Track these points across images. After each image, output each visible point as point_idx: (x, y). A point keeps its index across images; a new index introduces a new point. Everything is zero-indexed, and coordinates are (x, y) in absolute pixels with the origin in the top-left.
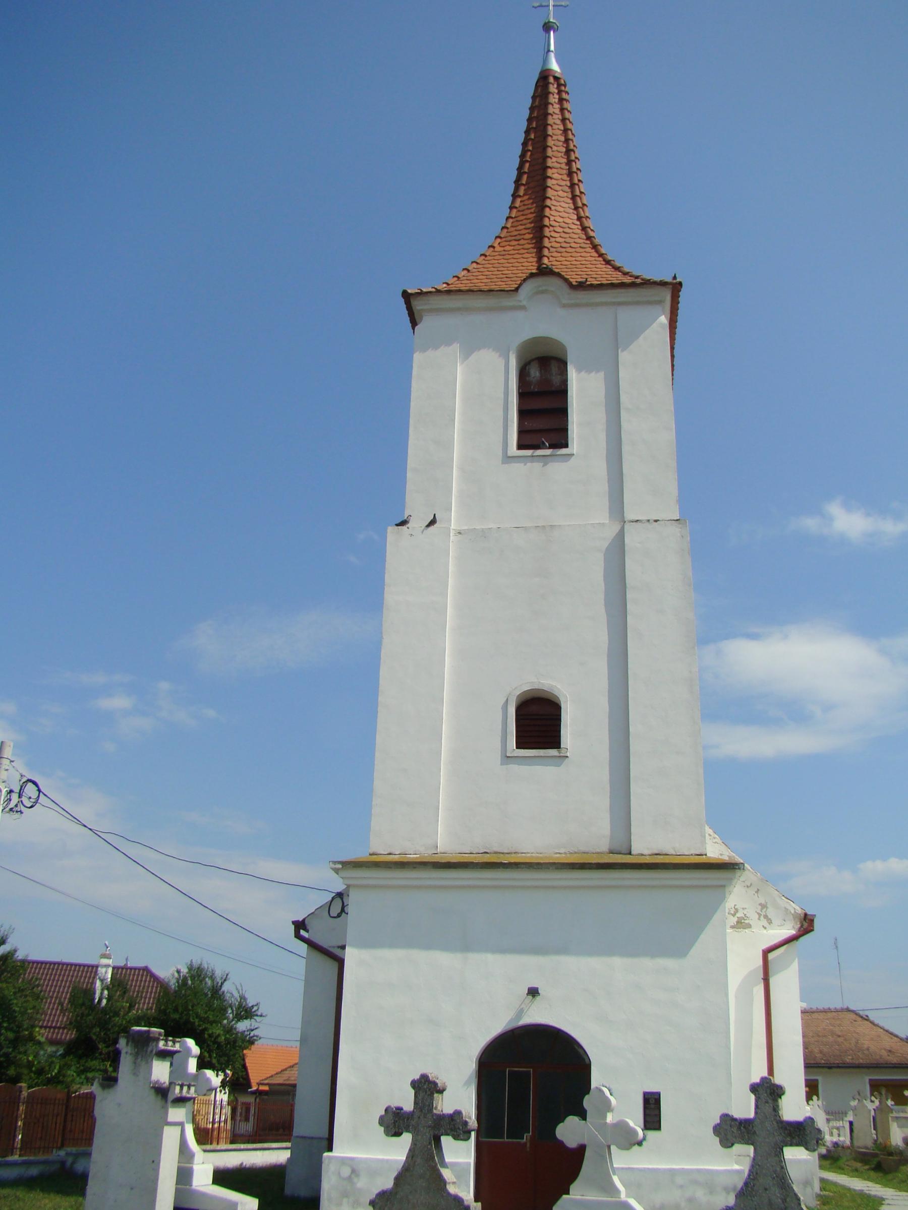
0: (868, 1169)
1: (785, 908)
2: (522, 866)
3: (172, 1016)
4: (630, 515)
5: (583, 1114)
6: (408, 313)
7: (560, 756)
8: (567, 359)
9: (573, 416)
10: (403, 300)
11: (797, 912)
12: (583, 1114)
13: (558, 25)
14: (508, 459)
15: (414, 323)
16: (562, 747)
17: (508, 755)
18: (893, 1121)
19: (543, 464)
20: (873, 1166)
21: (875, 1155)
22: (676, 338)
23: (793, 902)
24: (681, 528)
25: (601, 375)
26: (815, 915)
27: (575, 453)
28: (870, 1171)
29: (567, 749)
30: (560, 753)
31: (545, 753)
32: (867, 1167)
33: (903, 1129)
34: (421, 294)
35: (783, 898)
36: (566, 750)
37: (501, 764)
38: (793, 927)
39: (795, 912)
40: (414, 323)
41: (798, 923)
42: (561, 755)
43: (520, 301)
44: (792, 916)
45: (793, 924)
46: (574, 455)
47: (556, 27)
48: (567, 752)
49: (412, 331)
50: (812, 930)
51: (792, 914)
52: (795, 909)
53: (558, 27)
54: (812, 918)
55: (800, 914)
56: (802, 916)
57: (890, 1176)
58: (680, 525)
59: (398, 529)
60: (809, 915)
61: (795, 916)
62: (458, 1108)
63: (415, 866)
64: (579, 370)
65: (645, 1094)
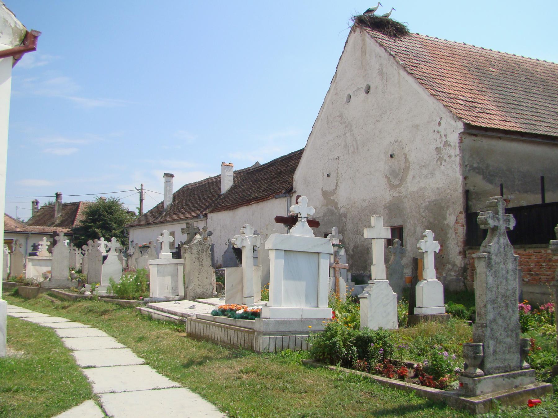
0: (9, 295)
1: (4, 19)
3: (444, 273)
5: (104, 240)
11: (18, 27)
12: (104, 240)
18: (29, 262)
20: (12, 293)
21: (14, 285)
23: (15, 16)
25: (304, 283)
26: (40, 32)
28: (10, 297)
32: (8, 293)
33: (37, 267)
35: (4, 8)
38: (11, 43)
39: (16, 26)
41: (18, 40)
44: (11, 31)
45: (11, 40)
50: (34, 49)
51: (12, 28)
52: (16, 23)
54: (36, 35)
55: (21, 30)
56: (24, 33)
57: (32, 301)
61: (15, 30)
65: (173, 258)
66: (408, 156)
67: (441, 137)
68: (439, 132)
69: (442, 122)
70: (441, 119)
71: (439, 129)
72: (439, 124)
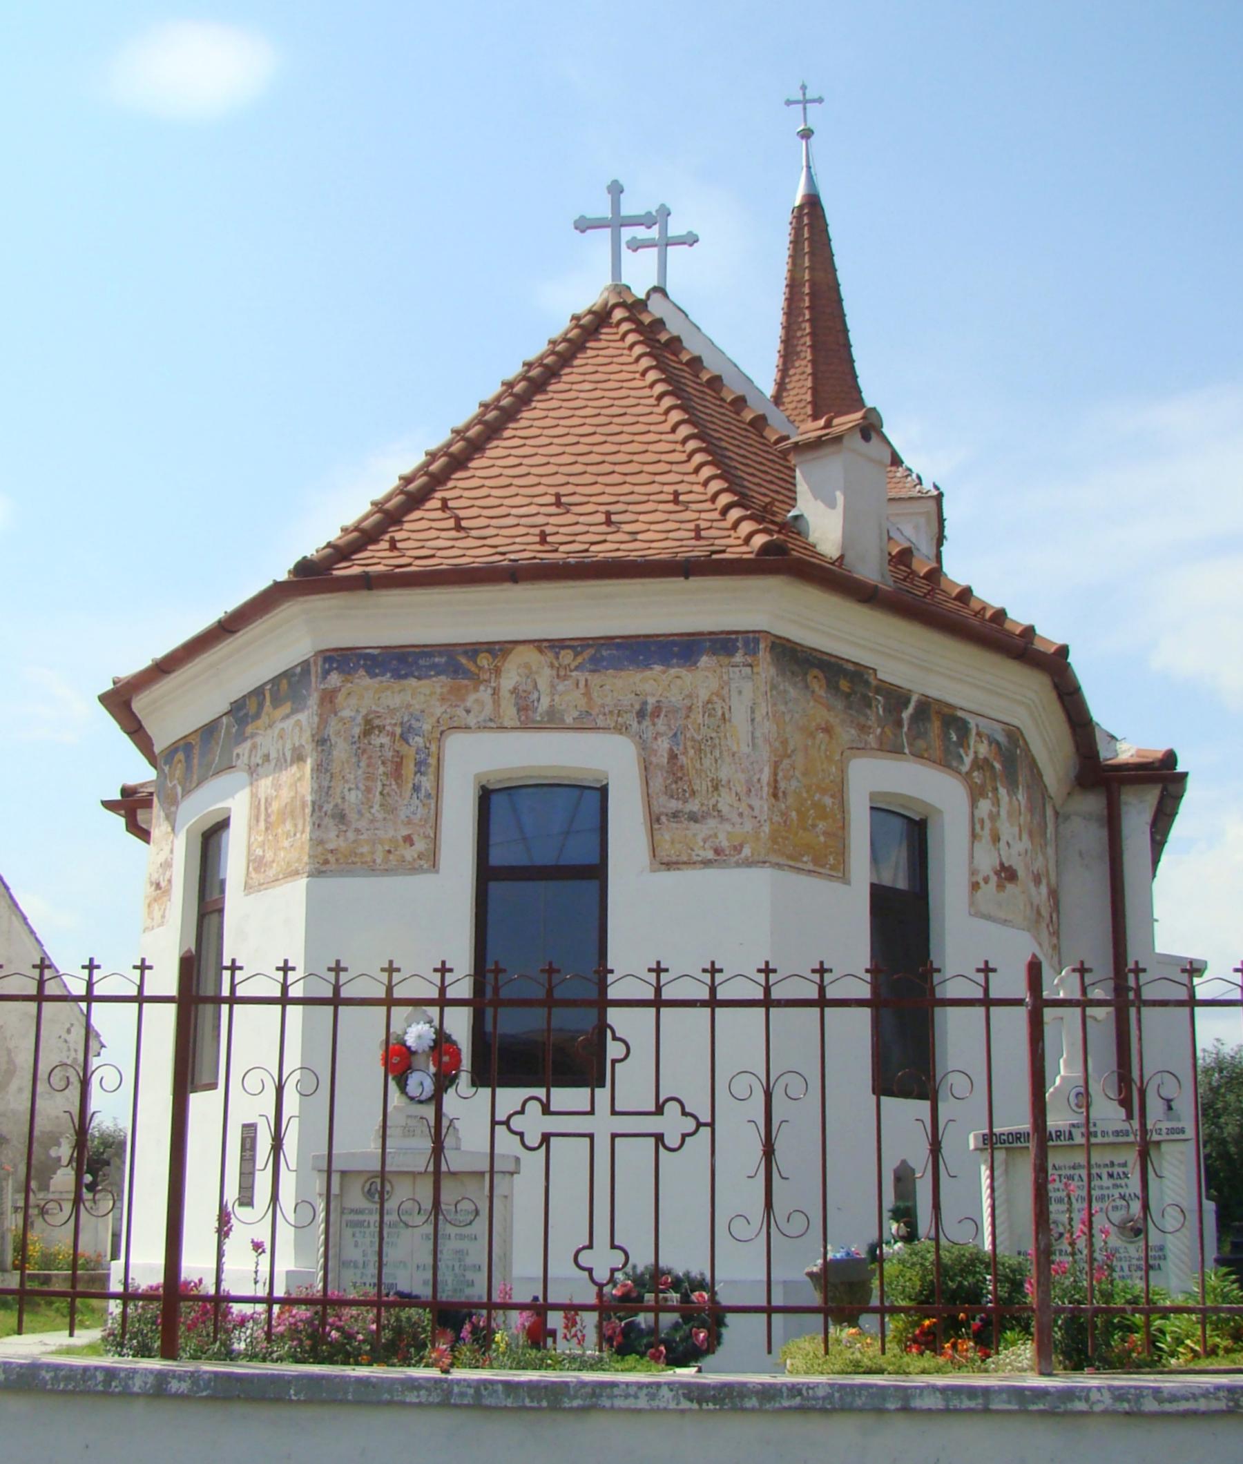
66: (13, 1055)
67: (69, 1050)
68: (66, 1041)
69: (72, 1030)
70: (72, 1025)
71: (68, 1037)
72: (69, 1031)
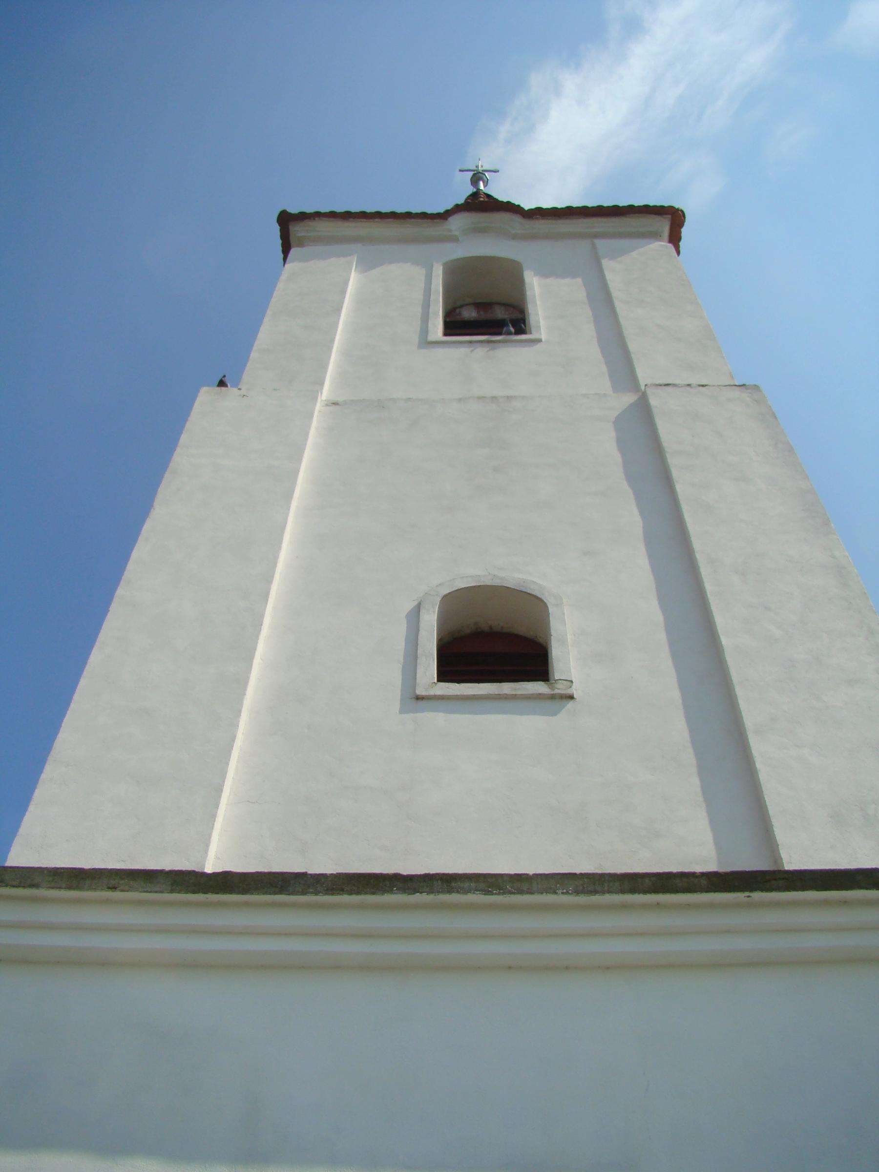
2: (466, 885)
4: (644, 375)
6: (282, 244)
7: (553, 697)
8: (548, 635)
9: (537, 314)
10: (278, 228)
13: (488, 178)
14: (426, 343)
15: (286, 249)
16: (557, 676)
17: (420, 691)
19: (488, 349)
22: (683, 235)
24: (750, 393)
27: (543, 340)
29: (572, 682)
30: (553, 689)
31: (515, 689)
34: (303, 217)
36: (569, 683)
37: (402, 711)
40: (286, 249)
42: (556, 691)
43: (450, 231)
46: (542, 341)
47: (486, 180)
48: (571, 687)
49: (282, 256)
53: (488, 179)
58: (749, 391)
59: (221, 389)
60: (748, 385)
62: (281, 209)
63: (113, 882)
64: (544, 273)
